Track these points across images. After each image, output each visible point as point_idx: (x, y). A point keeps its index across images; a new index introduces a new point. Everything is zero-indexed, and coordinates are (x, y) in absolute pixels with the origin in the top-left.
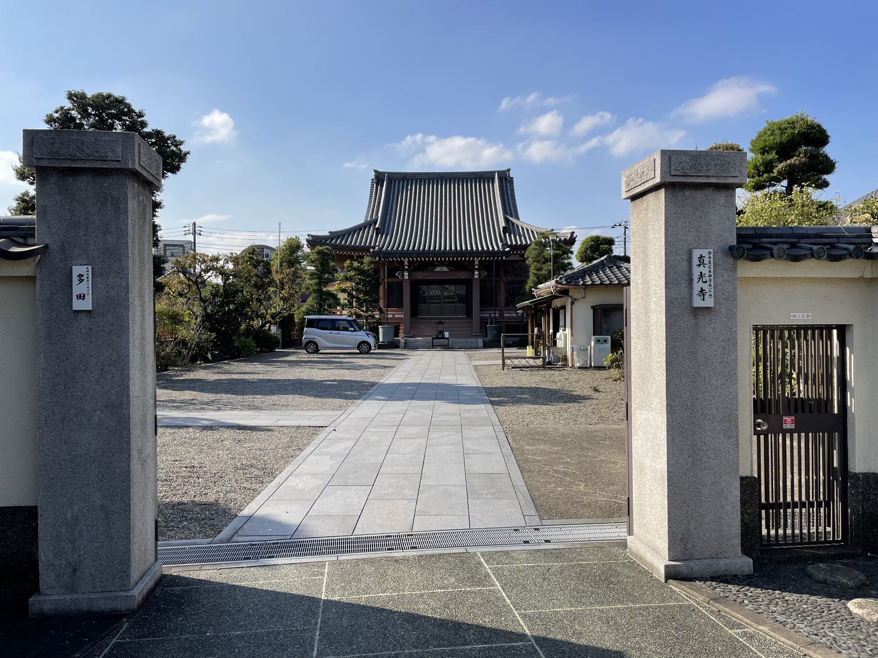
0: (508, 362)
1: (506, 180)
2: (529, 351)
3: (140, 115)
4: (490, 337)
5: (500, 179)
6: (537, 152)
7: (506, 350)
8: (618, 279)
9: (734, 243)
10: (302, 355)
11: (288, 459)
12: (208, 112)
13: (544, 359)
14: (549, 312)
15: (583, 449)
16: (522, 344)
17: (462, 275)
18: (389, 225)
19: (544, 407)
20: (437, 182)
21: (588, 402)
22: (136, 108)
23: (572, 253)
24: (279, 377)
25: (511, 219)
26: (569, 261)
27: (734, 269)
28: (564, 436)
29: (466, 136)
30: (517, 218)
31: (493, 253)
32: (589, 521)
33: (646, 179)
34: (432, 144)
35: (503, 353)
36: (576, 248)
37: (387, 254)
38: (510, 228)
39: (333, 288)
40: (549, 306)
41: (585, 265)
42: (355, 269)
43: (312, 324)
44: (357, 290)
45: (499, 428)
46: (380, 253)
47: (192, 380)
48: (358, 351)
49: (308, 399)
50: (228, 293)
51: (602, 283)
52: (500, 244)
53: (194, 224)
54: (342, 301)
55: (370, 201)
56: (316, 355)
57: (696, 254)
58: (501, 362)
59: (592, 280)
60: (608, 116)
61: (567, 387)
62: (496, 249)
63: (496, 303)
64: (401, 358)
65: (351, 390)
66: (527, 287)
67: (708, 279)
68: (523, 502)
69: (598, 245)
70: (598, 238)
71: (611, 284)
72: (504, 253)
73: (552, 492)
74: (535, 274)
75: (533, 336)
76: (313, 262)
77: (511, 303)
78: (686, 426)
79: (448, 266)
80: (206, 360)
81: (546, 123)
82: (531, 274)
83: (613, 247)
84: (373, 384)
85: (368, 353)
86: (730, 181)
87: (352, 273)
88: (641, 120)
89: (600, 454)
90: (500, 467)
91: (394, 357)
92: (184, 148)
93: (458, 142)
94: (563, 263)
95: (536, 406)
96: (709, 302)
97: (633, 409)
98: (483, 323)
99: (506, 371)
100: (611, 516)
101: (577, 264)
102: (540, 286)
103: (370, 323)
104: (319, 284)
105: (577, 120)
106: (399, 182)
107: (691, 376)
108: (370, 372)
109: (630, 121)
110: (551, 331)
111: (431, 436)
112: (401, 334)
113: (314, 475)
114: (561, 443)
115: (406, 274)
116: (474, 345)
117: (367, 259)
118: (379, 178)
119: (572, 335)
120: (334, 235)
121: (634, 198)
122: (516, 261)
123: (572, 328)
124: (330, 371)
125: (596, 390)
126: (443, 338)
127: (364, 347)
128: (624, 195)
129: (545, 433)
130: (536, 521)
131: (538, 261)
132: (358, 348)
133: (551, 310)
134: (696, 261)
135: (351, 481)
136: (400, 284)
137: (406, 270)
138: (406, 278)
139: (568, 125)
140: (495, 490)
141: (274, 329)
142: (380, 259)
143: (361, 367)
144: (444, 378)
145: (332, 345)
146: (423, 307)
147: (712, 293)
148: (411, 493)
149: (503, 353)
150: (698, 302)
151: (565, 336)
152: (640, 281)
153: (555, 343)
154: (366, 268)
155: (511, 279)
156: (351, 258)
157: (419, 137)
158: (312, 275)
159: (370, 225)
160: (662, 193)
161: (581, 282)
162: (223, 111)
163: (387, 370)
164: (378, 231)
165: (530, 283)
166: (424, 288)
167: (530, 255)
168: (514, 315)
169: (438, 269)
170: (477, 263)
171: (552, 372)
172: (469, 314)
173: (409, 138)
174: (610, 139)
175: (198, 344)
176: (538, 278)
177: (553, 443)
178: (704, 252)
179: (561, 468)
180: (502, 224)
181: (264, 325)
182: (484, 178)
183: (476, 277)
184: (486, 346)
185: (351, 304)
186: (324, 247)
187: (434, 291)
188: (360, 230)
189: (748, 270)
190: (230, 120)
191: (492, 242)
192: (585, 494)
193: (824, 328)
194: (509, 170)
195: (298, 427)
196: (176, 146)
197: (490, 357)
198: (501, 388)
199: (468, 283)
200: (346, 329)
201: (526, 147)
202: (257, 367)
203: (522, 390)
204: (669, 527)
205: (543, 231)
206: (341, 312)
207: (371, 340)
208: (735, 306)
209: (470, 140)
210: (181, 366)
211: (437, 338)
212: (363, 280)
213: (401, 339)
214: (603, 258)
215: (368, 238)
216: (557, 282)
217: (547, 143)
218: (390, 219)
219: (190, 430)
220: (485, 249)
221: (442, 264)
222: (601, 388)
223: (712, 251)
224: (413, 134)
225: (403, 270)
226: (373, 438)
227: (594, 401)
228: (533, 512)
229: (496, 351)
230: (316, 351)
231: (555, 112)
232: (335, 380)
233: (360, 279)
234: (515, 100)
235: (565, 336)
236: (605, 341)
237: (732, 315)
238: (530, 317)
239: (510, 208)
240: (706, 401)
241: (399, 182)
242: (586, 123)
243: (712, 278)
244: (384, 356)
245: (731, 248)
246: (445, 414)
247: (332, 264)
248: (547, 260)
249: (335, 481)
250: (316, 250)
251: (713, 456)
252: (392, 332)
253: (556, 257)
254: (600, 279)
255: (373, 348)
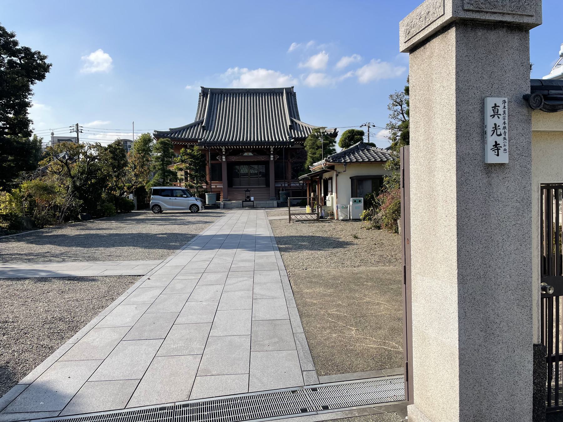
0: (293, 217)
1: (291, 94)
2: (308, 209)
3: (12, 36)
4: (282, 200)
5: (287, 94)
6: (313, 80)
7: (292, 208)
8: (368, 158)
9: (529, 92)
10: (150, 215)
11: (95, 310)
12: (94, 51)
13: (318, 214)
14: (321, 182)
15: (351, 290)
16: (303, 204)
17: (262, 158)
18: (212, 125)
19: (319, 252)
20: (245, 95)
21: (351, 247)
22: (9, 31)
23: (335, 142)
24: (126, 232)
25: (295, 120)
26: (334, 148)
27: (528, 121)
28: (335, 278)
29: (268, 69)
30: (299, 119)
31: (283, 143)
32: (364, 374)
33: (432, 19)
34: (245, 73)
35: (289, 210)
36: (338, 139)
37: (210, 144)
38: (294, 126)
39: (173, 168)
40: (321, 178)
41: (344, 149)
42: (188, 154)
43: (156, 192)
44: (190, 169)
45: (284, 273)
46: (205, 143)
47: (57, 235)
48: (190, 211)
49: (139, 250)
50: (90, 170)
51: (357, 161)
52: (287, 137)
53: (77, 125)
54: (179, 176)
55: (199, 108)
56: (160, 215)
57: (490, 102)
58: (288, 217)
59: (350, 159)
60: (359, 58)
61: (335, 235)
62: (285, 140)
63: (286, 177)
64: (220, 215)
65: (176, 242)
66: (306, 166)
67: (502, 131)
68: (301, 354)
69: (353, 136)
70: (353, 131)
71: (363, 161)
72: (290, 143)
73: (328, 338)
74: (311, 157)
75: (310, 199)
76: (158, 149)
77: (295, 176)
78: (478, 298)
79: (252, 152)
80: (77, 220)
81: (318, 60)
82: (308, 157)
83: (364, 137)
84: (193, 236)
85: (197, 212)
86: (526, 20)
87: (186, 157)
88: (379, 60)
89: (365, 295)
90: (282, 313)
91: (215, 215)
92: (47, 61)
93: (262, 72)
94: (330, 149)
95: (313, 252)
96: (504, 158)
97: (413, 273)
98: (277, 190)
99: (291, 223)
100: (382, 368)
101: (339, 149)
102: (315, 164)
103: (199, 192)
104: (162, 164)
105: (338, 59)
106: (218, 95)
107: (483, 241)
108: (194, 226)
109: (373, 61)
110: (323, 195)
111: (229, 281)
112: (221, 199)
113: (114, 328)
114: (333, 285)
115: (224, 157)
116: (271, 205)
117: (196, 148)
118: (205, 92)
119: (337, 197)
120: (173, 131)
121: (412, 49)
122: (299, 149)
123: (337, 193)
124: (165, 226)
125: (356, 237)
126: (250, 201)
127: (195, 208)
128: (403, 46)
129: (320, 276)
130: (313, 378)
131: (313, 148)
132: (190, 209)
133: (322, 181)
134: (489, 111)
135: (146, 335)
136: (220, 164)
137: (224, 155)
138: (224, 160)
139: (332, 63)
140: (276, 340)
141: (131, 196)
142: (205, 147)
143: (189, 223)
144: (248, 230)
145: (172, 207)
146: (236, 180)
147: (507, 148)
148: (197, 346)
149: (289, 210)
150: (491, 158)
151: (332, 198)
152: (421, 138)
153: (325, 203)
154: (196, 154)
155: (295, 160)
156: (186, 147)
157: (236, 69)
158: (157, 158)
159: (199, 124)
160: (452, 33)
161: (343, 161)
162: (105, 52)
163: (207, 225)
164: (204, 128)
165: (308, 163)
166: (237, 167)
167: (308, 144)
168: (298, 185)
169: (246, 154)
170: (272, 149)
171: (324, 224)
172: (268, 185)
173: (230, 70)
174: (359, 72)
175: (68, 208)
176: (313, 159)
177: (327, 285)
178: (499, 101)
179: (333, 311)
180: (289, 123)
181: (122, 194)
182: (276, 92)
183: (272, 159)
184: (279, 206)
185: (186, 178)
186: (165, 139)
187: (244, 170)
188: (192, 127)
189: (544, 122)
190: (110, 58)
191: (283, 136)
192: (357, 340)
193: (553, 187)
194: (293, 87)
195: (120, 277)
196: (41, 60)
197: (281, 214)
198: (287, 237)
199: (266, 163)
200: (181, 196)
201: (306, 77)
202: (114, 224)
203: (303, 238)
204: (460, 410)
205: (316, 128)
206: (180, 184)
207: (199, 204)
208: (530, 163)
209: (270, 71)
210: (56, 224)
211: (246, 201)
212: (194, 162)
213: (221, 202)
214: (357, 144)
215: (197, 134)
216: (326, 160)
217: (319, 75)
218: (212, 120)
219: (27, 282)
220: (278, 140)
221: (248, 150)
222: (359, 235)
223: (506, 99)
224: (233, 67)
225: (222, 155)
226: (179, 286)
227: (355, 246)
228: (310, 366)
229: (286, 209)
230: (160, 211)
231: (324, 52)
232: (166, 234)
233: (191, 161)
234: (299, 45)
235: (332, 198)
236: (360, 201)
237: (526, 173)
238: (308, 185)
239: (294, 112)
240: (499, 268)
241: (218, 95)
242: (344, 62)
243: (507, 131)
244: (208, 214)
245: (526, 98)
246: (243, 261)
247: (171, 151)
248: (319, 147)
249: (128, 337)
250: (159, 141)
251: (506, 329)
252: (215, 198)
253: (325, 145)
254: (356, 158)
255: (200, 209)
